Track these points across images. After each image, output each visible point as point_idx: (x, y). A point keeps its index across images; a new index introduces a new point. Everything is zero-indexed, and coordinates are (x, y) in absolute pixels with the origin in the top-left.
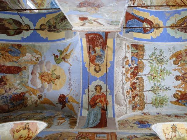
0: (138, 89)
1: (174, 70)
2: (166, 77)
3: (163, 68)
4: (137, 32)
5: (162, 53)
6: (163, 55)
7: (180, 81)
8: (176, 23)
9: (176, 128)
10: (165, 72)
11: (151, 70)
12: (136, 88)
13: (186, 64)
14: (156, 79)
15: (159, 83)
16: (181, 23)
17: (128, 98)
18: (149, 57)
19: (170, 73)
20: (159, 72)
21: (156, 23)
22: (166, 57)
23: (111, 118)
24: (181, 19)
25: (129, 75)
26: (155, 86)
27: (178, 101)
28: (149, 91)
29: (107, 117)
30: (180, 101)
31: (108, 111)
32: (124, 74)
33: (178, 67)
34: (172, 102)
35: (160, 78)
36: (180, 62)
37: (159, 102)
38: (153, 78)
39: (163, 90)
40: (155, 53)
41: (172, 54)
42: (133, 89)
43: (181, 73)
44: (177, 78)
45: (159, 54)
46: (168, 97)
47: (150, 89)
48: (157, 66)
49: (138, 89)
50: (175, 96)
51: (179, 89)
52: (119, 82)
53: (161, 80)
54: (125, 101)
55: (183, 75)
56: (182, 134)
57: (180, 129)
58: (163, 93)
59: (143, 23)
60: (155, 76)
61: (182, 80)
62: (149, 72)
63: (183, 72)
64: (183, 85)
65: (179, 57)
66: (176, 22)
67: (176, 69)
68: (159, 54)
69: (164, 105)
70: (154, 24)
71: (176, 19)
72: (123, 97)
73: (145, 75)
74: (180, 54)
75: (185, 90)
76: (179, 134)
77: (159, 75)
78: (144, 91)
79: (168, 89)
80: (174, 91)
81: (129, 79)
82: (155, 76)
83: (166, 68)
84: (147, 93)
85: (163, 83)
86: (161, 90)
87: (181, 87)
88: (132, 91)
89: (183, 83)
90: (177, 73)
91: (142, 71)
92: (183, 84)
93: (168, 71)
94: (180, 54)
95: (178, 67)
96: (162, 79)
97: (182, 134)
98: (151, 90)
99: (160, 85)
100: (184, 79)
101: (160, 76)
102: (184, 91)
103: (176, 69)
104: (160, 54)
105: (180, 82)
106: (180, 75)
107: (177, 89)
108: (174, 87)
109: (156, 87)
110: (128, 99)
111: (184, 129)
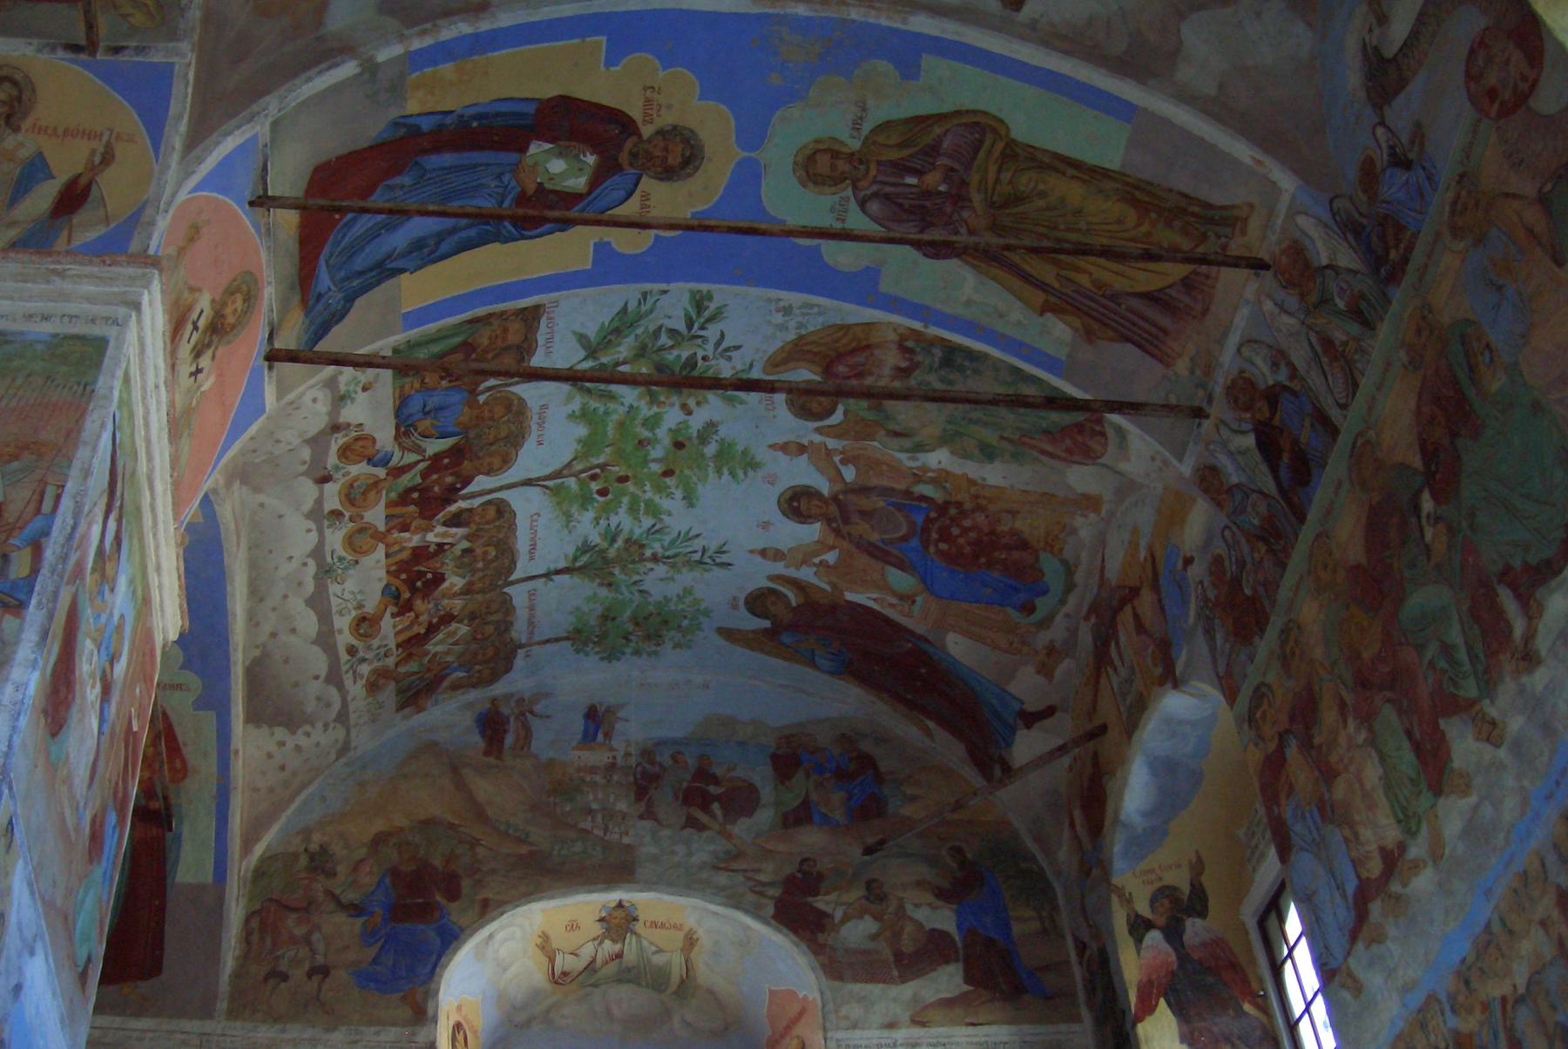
0: (453, 585)
1: (784, 448)
2: (712, 489)
3: (697, 421)
4: (450, 255)
5: (710, 319)
6: (712, 332)
7: (818, 525)
8: (855, 145)
9: (636, 919)
10: (710, 450)
11: (588, 446)
12: (439, 579)
13: (883, 432)
14: (625, 500)
15: (647, 522)
16: (905, 153)
17: (363, 660)
18: (582, 354)
19: (751, 464)
20: (657, 452)
21: (667, 119)
22: (733, 354)
23: (202, 887)
24: (907, 121)
25: (376, 515)
26: (613, 540)
27: (772, 633)
28: (558, 572)
29: (169, 881)
30: (786, 638)
31: (186, 830)
32: (336, 514)
33: (817, 438)
34: (728, 634)
35: (659, 489)
36: (840, 409)
37: (630, 627)
38: (603, 492)
39: (673, 566)
40: (639, 317)
41: (791, 336)
42: (413, 590)
43: (830, 481)
44: (797, 504)
45: (681, 326)
46: (703, 606)
47: (562, 564)
48: (646, 411)
49: (455, 581)
50: (757, 602)
51: (792, 572)
52: (287, 568)
53: (672, 504)
54: (340, 686)
55: (845, 492)
56: (660, 951)
57: (654, 925)
58: (673, 579)
59: (523, 149)
60: (623, 479)
61: (829, 521)
62: (567, 458)
63: (849, 473)
64: (831, 557)
65: (841, 369)
66: (867, 128)
67: (802, 449)
68: (681, 326)
69: (668, 646)
70: (647, 131)
71: (871, 103)
72: (320, 663)
73: (528, 483)
74: (853, 352)
75: (834, 586)
76: (641, 949)
77: (656, 468)
78: (513, 583)
79: (716, 559)
80: (759, 575)
81: (379, 537)
82: (623, 479)
83: (723, 431)
84: (532, 594)
85: (678, 518)
86: (655, 558)
87: (817, 560)
88: (404, 608)
89: (831, 540)
90: (804, 473)
91: (507, 462)
92: (832, 548)
93: (740, 448)
94: (853, 352)
95: (817, 438)
96: (679, 494)
97: (660, 951)
98: (578, 564)
99: (651, 531)
100: (846, 521)
101: (668, 473)
102: (828, 588)
103: (802, 449)
104: (690, 325)
105: (812, 532)
106: (825, 488)
107: (779, 568)
108: (763, 553)
109: (619, 543)
110: (365, 669)
111: (676, 927)
